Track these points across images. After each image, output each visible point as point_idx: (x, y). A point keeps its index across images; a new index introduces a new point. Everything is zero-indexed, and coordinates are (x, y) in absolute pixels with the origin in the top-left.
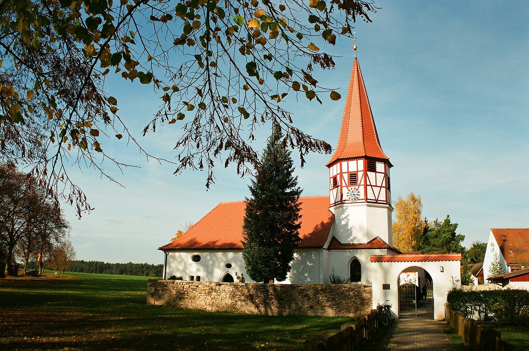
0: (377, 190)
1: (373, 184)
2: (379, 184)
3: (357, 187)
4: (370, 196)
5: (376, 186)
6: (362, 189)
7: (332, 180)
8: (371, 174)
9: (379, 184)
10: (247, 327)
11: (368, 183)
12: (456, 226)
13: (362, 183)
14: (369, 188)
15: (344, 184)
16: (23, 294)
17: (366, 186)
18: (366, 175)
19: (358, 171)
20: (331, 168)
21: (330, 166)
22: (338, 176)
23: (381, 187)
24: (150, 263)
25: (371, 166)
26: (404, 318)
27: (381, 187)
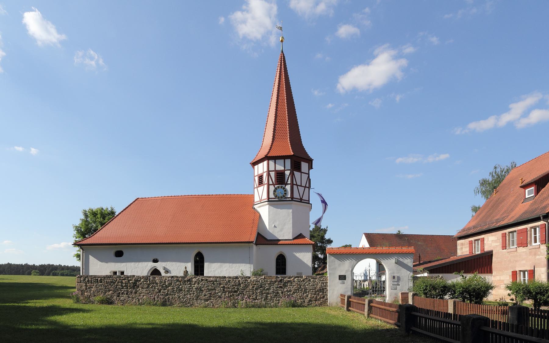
0: (301, 189)
1: (299, 184)
2: (303, 185)
3: (284, 186)
4: (296, 195)
5: (301, 186)
6: (288, 187)
7: (257, 178)
8: (297, 174)
9: (303, 185)
10: (39, 303)
11: (295, 183)
12: (325, 231)
13: (289, 182)
14: (295, 187)
15: (271, 183)
16: (12, 306)
17: (292, 185)
18: (292, 174)
19: (285, 170)
20: (256, 167)
21: (254, 164)
22: (265, 175)
23: (305, 187)
24: (31, 263)
25: (296, 167)
26: (512, 210)
27: (305, 187)
